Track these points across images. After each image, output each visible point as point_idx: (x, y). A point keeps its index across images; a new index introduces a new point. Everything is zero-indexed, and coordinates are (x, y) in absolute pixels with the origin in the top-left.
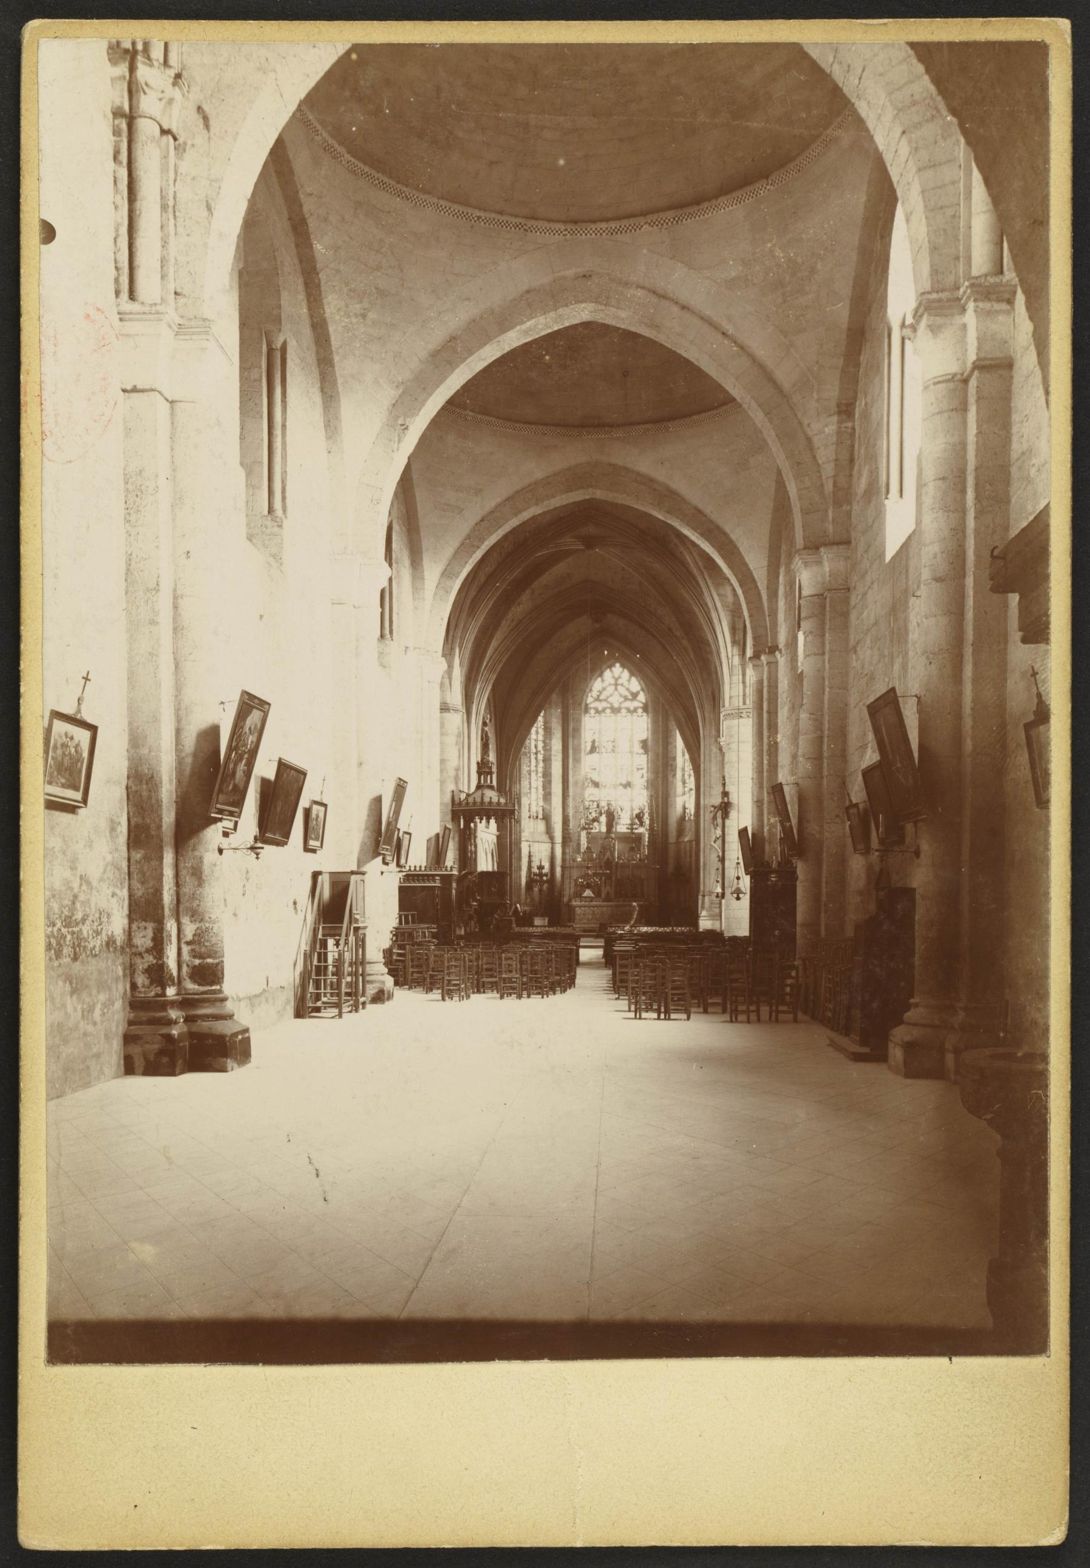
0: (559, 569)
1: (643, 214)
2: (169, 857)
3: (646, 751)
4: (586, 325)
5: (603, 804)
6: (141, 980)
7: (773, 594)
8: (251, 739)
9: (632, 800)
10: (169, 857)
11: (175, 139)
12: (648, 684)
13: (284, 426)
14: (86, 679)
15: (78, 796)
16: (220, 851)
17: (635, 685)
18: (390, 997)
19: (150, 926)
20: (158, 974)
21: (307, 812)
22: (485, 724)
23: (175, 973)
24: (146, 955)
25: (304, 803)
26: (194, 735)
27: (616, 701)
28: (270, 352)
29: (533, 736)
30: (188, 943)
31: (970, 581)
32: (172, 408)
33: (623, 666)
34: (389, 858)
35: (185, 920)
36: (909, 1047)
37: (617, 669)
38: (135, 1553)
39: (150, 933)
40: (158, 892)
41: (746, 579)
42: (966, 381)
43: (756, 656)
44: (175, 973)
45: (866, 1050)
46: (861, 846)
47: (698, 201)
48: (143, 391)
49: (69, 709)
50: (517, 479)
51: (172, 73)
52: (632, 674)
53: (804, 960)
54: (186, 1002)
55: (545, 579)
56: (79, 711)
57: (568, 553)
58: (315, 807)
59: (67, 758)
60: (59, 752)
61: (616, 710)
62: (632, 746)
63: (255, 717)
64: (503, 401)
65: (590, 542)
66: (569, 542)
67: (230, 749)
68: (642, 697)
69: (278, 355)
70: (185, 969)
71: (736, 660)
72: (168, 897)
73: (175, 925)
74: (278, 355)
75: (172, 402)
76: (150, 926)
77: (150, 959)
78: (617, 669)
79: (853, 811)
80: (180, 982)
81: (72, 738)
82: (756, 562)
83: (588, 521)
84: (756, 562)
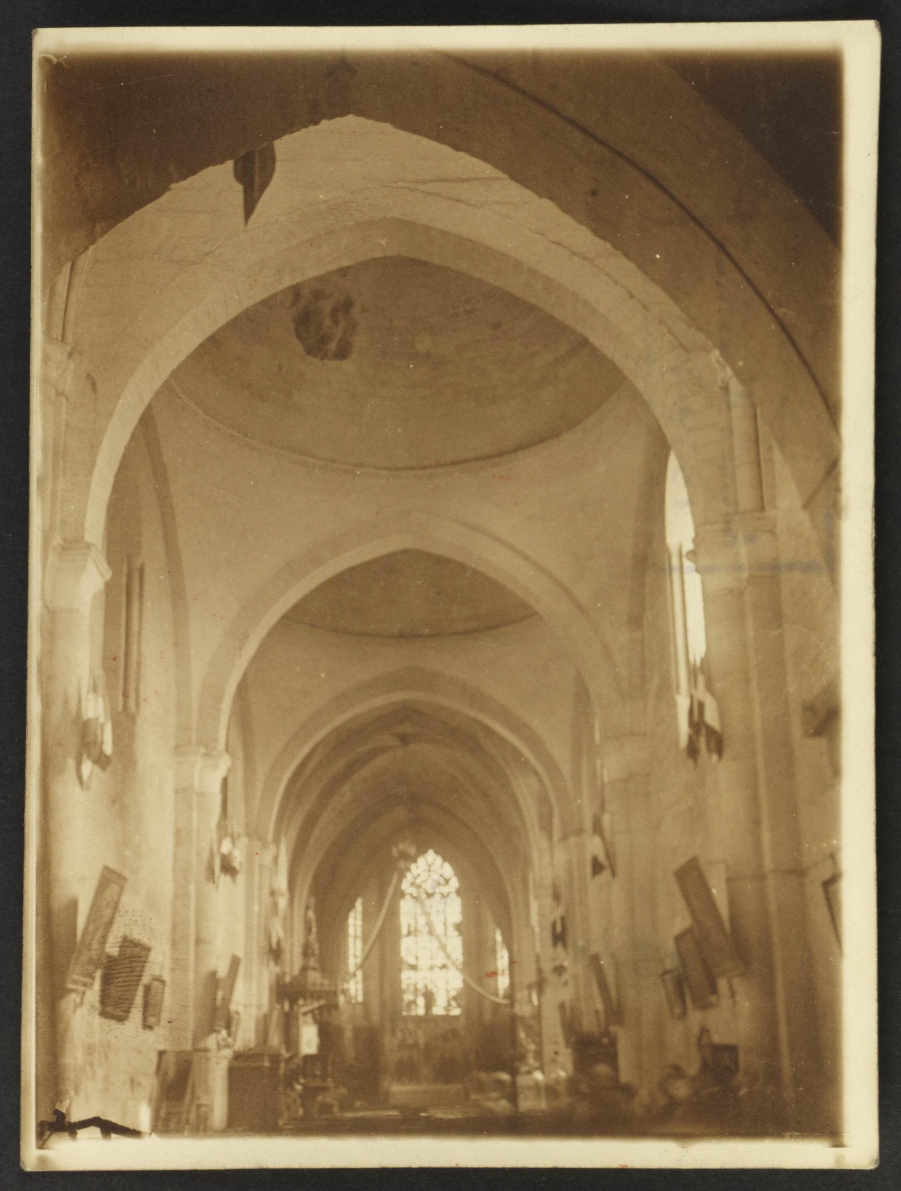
0: (379, 762)
1: (454, 463)
3: (461, 934)
4: (404, 552)
5: (420, 986)
7: (577, 780)
8: (108, 912)
9: (447, 983)
11: (67, 399)
12: (459, 872)
13: (140, 635)
17: (448, 870)
21: (148, 989)
22: (307, 908)
25: (145, 980)
27: (428, 886)
29: (351, 921)
31: (760, 758)
33: (437, 852)
37: (431, 855)
38: (503, 1170)
41: (553, 769)
42: (741, 594)
43: (564, 838)
46: (677, 1011)
47: (501, 454)
50: (333, 687)
51: (68, 348)
52: (445, 860)
55: (366, 772)
57: (383, 750)
58: (156, 984)
61: (430, 897)
63: (113, 889)
64: (340, 611)
65: (405, 739)
67: (90, 920)
68: (455, 883)
69: (136, 575)
71: (544, 844)
74: (136, 575)
78: (431, 855)
79: (668, 977)
82: (561, 754)
83: (406, 722)
84: (561, 754)
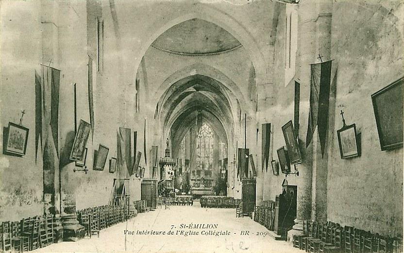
2: (57, 172)
6: (48, 212)
10: (57, 172)
14: (23, 113)
15: (22, 152)
16: (74, 171)
18: (137, 215)
19: (50, 195)
20: (53, 211)
21: (110, 161)
23: (59, 210)
24: (49, 204)
26: (66, 134)
28: (99, 23)
30: (63, 200)
32: (58, 29)
34: (138, 175)
35: (62, 193)
36: (295, 237)
39: (50, 197)
40: (53, 184)
44: (59, 210)
45: (280, 236)
46: (276, 173)
48: (47, 23)
49: (17, 123)
53: (258, 207)
54: (63, 219)
56: (21, 123)
59: (16, 139)
60: (13, 137)
62: (209, 147)
66: (191, 89)
69: (101, 24)
70: (62, 208)
72: (56, 186)
73: (59, 195)
75: (58, 27)
76: (50, 195)
77: (50, 205)
80: (61, 213)
81: (18, 132)
